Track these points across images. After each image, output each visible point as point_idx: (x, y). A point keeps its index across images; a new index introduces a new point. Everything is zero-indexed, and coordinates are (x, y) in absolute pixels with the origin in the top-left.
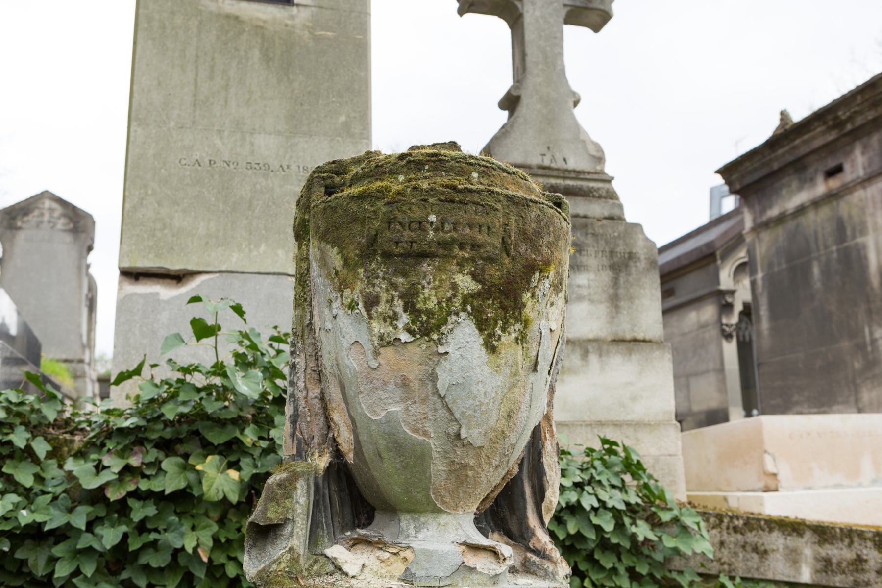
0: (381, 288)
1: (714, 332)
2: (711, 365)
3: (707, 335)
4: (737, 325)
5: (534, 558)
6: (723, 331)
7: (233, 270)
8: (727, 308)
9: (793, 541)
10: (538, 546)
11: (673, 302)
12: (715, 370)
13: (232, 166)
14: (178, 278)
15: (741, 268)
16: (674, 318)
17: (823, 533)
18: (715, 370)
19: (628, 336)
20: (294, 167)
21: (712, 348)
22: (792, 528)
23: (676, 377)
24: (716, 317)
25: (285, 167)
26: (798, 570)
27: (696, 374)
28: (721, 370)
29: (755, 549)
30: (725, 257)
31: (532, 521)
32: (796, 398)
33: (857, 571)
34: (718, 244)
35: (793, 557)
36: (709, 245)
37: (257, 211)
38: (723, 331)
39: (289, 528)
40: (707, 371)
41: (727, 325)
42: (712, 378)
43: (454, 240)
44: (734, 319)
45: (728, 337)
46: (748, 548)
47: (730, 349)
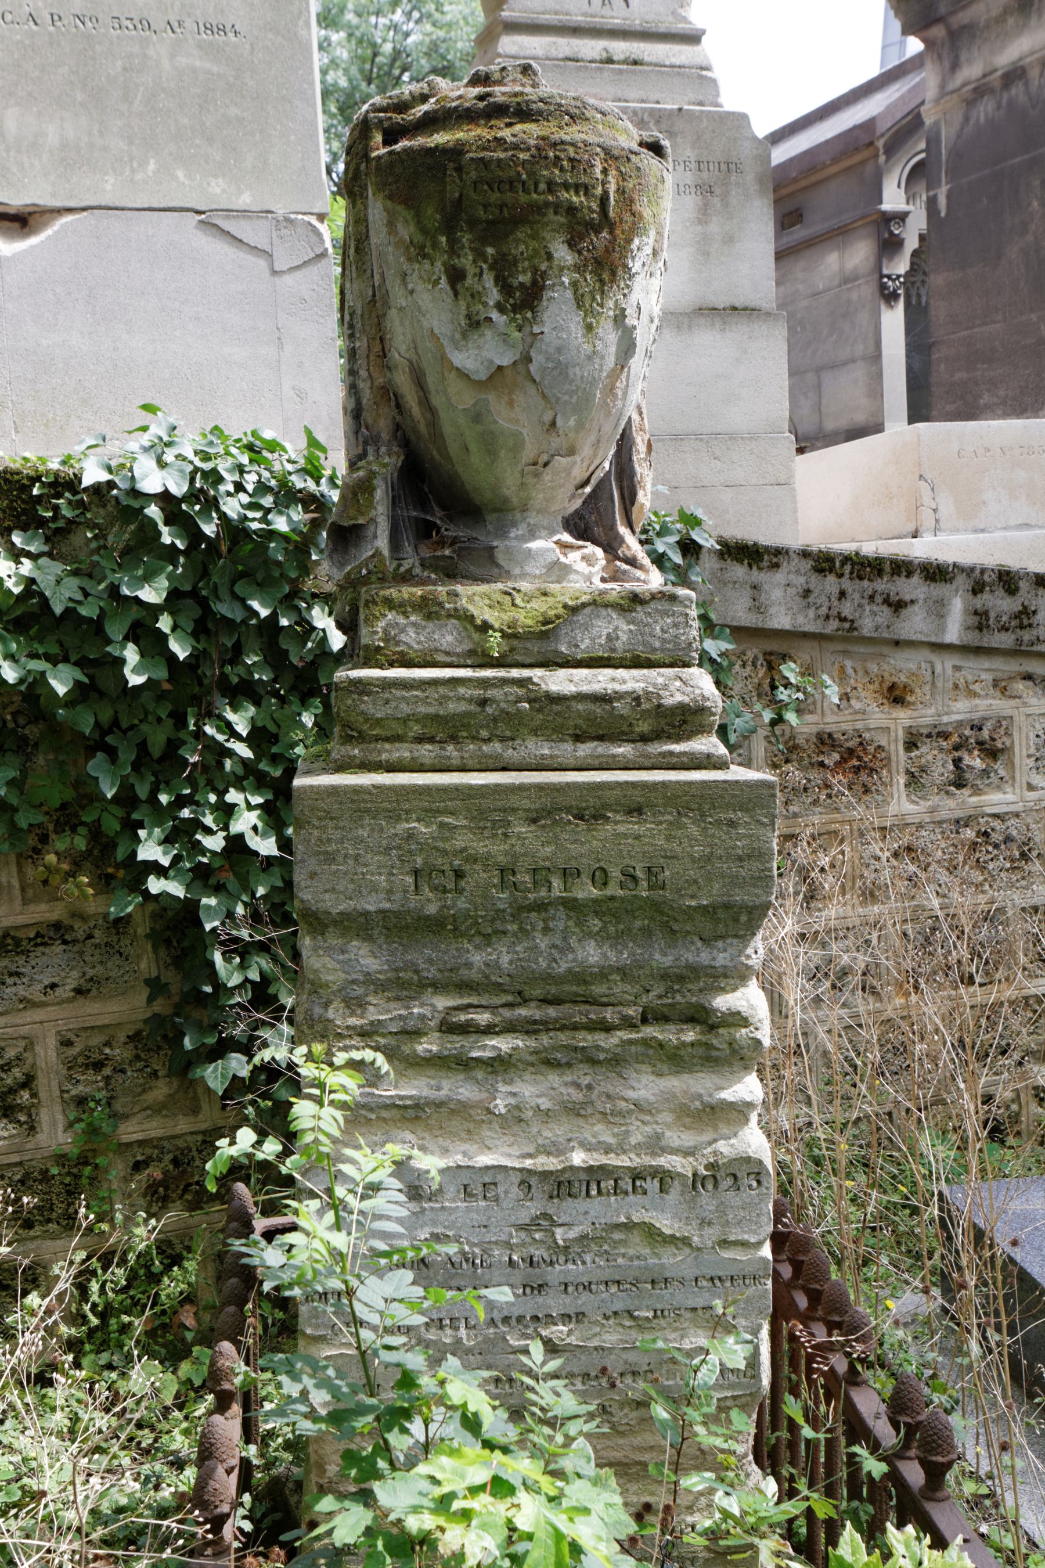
0: (466, 261)
1: (867, 290)
2: (859, 349)
3: (855, 295)
4: (907, 275)
5: (625, 567)
6: (883, 287)
7: (118, 204)
8: (891, 245)
9: (939, 590)
10: (628, 554)
11: (799, 233)
12: (864, 358)
13: (89, 24)
15: (917, 172)
16: (798, 267)
17: (980, 581)
18: (864, 358)
19: (722, 302)
20: (189, 24)
21: (863, 318)
22: (936, 573)
23: (793, 372)
24: (872, 260)
25: (175, 25)
26: (942, 629)
27: (834, 366)
28: (876, 357)
29: (887, 601)
30: (892, 148)
31: (623, 530)
32: (985, 399)
33: (1022, 627)
34: (882, 127)
35: (939, 610)
36: (868, 126)
37: (137, 103)
38: (883, 287)
39: (372, 528)
40: (853, 361)
41: (889, 277)
42: (859, 372)
43: (547, 204)
44: (901, 266)
45: (890, 298)
46: (879, 599)
47: (893, 322)
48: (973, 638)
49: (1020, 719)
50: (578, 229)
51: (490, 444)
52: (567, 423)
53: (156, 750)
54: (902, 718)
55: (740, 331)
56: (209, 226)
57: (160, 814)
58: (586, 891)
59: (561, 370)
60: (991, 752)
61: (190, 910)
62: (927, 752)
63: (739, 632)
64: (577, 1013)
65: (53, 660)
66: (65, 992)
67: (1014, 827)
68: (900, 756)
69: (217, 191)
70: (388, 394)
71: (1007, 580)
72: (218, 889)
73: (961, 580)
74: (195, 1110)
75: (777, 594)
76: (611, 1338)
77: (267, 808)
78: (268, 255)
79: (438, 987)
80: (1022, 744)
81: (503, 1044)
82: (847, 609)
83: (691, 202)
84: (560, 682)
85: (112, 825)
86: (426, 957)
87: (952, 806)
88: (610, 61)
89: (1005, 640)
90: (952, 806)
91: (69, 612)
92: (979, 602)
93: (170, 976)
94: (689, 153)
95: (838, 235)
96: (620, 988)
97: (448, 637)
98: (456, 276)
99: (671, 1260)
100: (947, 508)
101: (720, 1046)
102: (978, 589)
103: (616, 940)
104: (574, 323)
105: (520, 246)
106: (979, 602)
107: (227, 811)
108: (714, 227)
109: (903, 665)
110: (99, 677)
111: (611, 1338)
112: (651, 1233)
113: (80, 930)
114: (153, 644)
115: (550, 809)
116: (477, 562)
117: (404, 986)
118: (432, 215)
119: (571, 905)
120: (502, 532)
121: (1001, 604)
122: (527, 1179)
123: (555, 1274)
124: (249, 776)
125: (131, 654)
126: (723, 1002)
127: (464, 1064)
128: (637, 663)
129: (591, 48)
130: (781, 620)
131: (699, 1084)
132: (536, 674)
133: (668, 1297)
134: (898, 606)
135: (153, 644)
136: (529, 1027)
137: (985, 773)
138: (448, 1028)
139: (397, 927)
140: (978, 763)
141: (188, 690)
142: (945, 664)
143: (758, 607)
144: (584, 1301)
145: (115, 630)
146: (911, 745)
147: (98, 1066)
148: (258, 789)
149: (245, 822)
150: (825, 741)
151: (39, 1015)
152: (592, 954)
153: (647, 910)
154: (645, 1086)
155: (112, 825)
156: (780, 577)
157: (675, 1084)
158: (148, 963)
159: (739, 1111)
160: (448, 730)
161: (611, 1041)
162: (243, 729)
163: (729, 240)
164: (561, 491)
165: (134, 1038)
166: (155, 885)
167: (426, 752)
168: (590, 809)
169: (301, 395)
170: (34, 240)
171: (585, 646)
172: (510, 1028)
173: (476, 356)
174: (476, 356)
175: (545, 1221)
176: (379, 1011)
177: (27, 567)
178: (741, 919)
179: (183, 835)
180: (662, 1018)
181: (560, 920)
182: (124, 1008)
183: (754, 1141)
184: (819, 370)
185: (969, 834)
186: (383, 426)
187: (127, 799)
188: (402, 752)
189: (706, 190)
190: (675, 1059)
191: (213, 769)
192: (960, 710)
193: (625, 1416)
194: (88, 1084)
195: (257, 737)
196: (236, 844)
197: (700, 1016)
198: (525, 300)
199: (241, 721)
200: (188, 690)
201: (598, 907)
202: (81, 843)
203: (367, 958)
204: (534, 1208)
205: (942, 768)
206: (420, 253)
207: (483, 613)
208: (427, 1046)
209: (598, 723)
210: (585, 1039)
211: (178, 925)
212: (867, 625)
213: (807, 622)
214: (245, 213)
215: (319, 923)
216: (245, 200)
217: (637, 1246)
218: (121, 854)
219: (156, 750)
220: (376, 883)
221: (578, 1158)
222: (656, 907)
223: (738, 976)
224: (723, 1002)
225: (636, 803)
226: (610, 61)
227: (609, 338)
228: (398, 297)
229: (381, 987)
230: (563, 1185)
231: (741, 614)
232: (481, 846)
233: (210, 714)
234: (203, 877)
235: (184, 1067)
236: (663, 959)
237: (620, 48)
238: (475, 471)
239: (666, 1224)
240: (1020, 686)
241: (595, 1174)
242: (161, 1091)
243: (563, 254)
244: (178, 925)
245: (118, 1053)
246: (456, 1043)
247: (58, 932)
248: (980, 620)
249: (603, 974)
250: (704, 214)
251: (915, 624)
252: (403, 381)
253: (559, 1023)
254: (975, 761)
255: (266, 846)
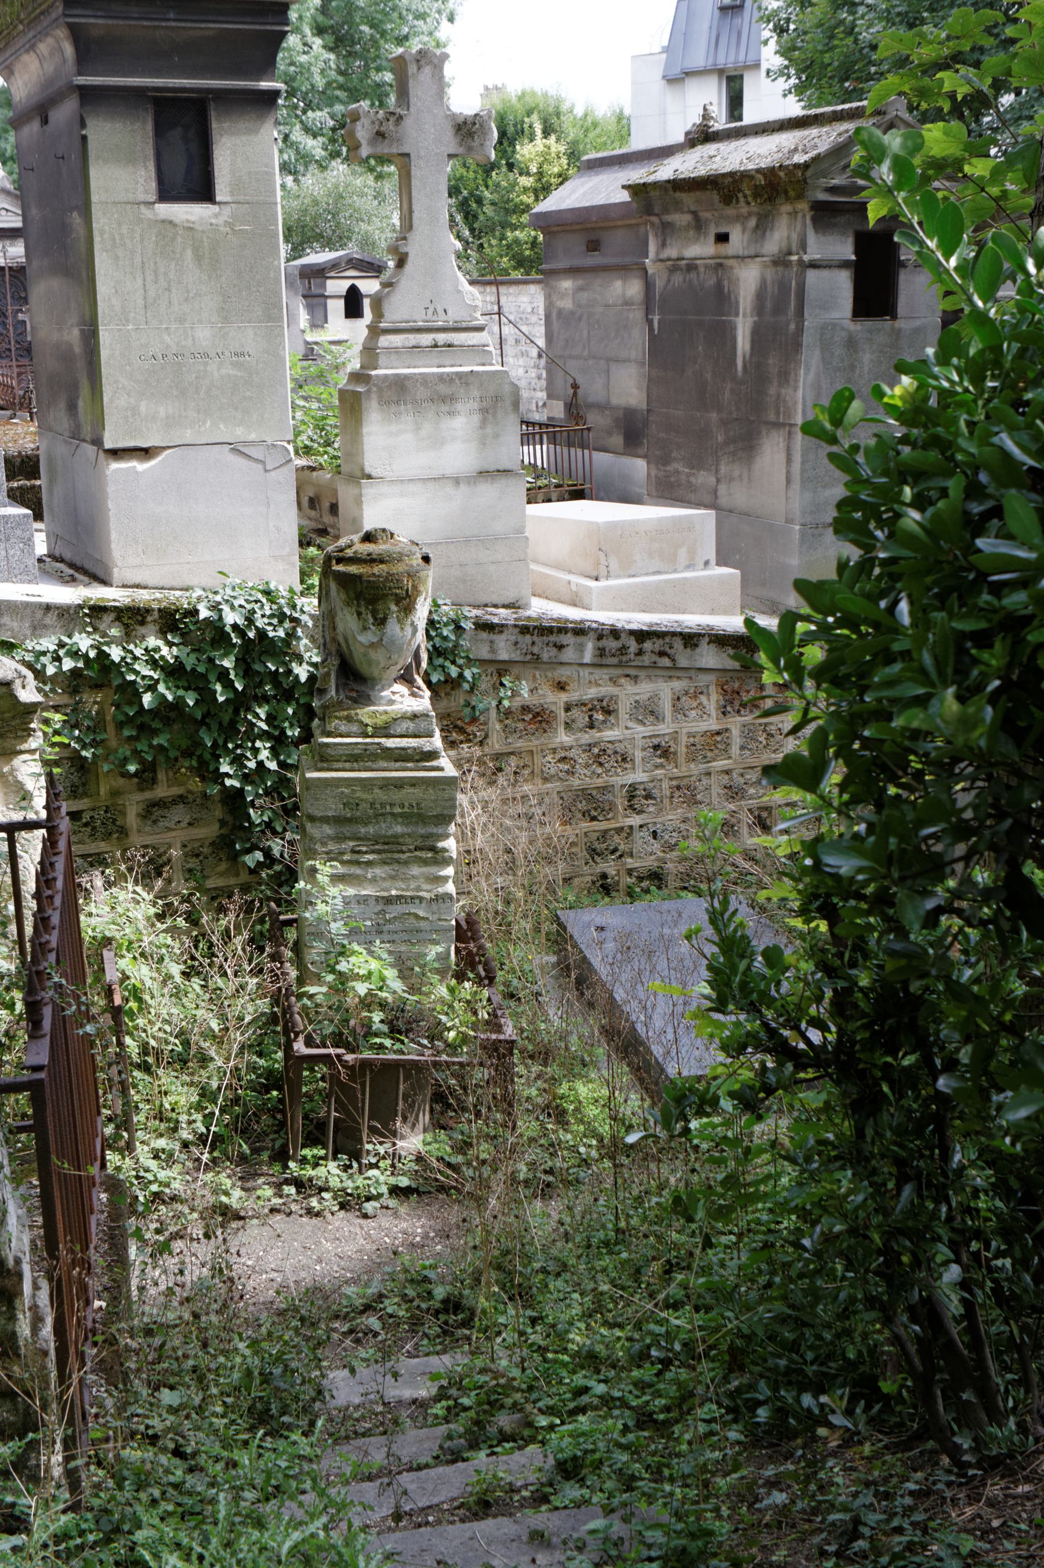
9: (580, 639)
14: (145, 453)
35: (581, 648)
48: (597, 660)
49: (622, 696)
50: (398, 600)
51: (370, 663)
52: (395, 657)
53: (225, 723)
54: (564, 697)
55: (502, 483)
56: (236, 451)
57: (228, 752)
58: (397, 810)
59: (393, 642)
60: (607, 712)
61: (240, 792)
62: (575, 713)
63: (482, 662)
64: (394, 847)
65: (186, 689)
66: (184, 824)
67: (620, 747)
68: (562, 715)
69: (239, 433)
70: (334, 640)
71: (615, 633)
72: (252, 783)
73: (591, 634)
74: (237, 875)
75: (502, 644)
76: (403, 948)
77: (272, 748)
78: (263, 463)
79: (350, 839)
80: (624, 708)
81: (370, 857)
82: (536, 650)
83: (476, 418)
84: (391, 743)
85: (207, 756)
86: (347, 830)
87: (586, 738)
88: (436, 346)
89: (614, 661)
90: (586, 738)
91: (194, 670)
92: (601, 644)
93: (229, 818)
94: (476, 393)
95: (622, 270)
96: (408, 840)
97: (354, 728)
98: (359, 614)
99: (423, 924)
100: (614, 564)
101: (440, 858)
102: (600, 637)
103: (407, 825)
104: (397, 628)
105: (380, 606)
106: (601, 644)
107: (256, 751)
108: (489, 430)
109: (563, 673)
110: (206, 696)
111: (403, 948)
112: (417, 916)
113: (191, 798)
114: (228, 685)
115: (386, 784)
116: (364, 699)
117: (340, 838)
118: (352, 594)
119: (392, 814)
120: (373, 688)
121: (612, 644)
122: (377, 899)
123: (386, 928)
124: (264, 735)
125: (218, 687)
126: (440, 845)
127: (358, 863)
128: (415, 736)
129: (426, 339)
130: (504, 656)
131: (432, 870)
132: (382, 740)
133: (421, 936)
134: (560, 647)
135: (228, 685)
136: (378, 852)
137: (604, 722)
138: (353, 852)
139: (338, 821)
140: (601, 717)
141: (240, 703)
142: (585, 673)
143: (493, 651)
144: (395, 937)
145: (212, 677)
146: (568, 709)
147: (197, 856)
148: (268, 740)
149: (264, 754)
150: (525, 709)
151: (174, 834)
152: (399, 829)
153: (416, 816)
154: (415, 870)
155: (207, 756)
156: (503, 637)
157: (425, 870)
158: (218, 812)
159: (445, 879)
160: (356, 758)
161: (404, 856)
162: (263, 716)
163: (496, 436)
164: (394, 671)
165: (212, 844)
166: (228, 782)
167: (347, 765)
168: (399, 784)
169: (278, 529)
170: (153, 463)
171: (399, 730)
172: (373, 852)
173: (365, 638)
174: (365, 638)
175: (383, 912)
176: (332, 846)
177: (175, 649)
178: (445, 818)
179: (238, 761)
180: (421, 849)
181: (389, 819)
182: (209, 831)
183: (450, 888)
184: (609, 360)
185: (596, 750)
186: (333, 649)
187: (215, 744)
188: (340, 765)
189: (484, 411)
190: (425, 862)
191: (252, 734)
192: (592, 693)
193: (407, 973)
194: (193, 863)
195: (270, 719)
196: (260, 764)
197: (433, 849)
198: (381, 622)
199: (262, 712)
200: (240, 703)
201: (401, 815)
202: (195, 763)
203: (328, 830)
204: (379, 908)
205: (582, 719)
206: (348, 604)
207: (367, 720)
208: (346, 857)
209: (402, 756)
210: (396, 856)
211: (234, 800)
212: (545, 657)
213: (516, 656)
214: (252, 443)
215: (312, 819)
216: (253, 437)
217: (412, 920)
218: (212, 768)
219: (225, 723)
220: (332, 807)
221: (394, 892)
222: (419, 815)
223: (447, 836)
224: (440, 845)
225: (414, 782)
226: (436, 346)
227: (409, 630)
228: (340, 615)
229: (332, 839)
230: (389, 901)
231: (484, 653)
232: (364, 796)
233: (249, 709)
234: (246, 778)
235: (234, 857)
236: (422, 830)
237: (442, 338)
238: (364, 669)
239: (421, 913)
240: (623, 680)
241: (399, 898)
242: (223, 866)
243: (394, 608)
244: (234, 800)
245: (206, 850)
246: (356, 857)
247: (181, 799)
248: (601, 652)
249: (403, 835)
250: (484, 423)
251: (568, 655)
252: (341, 639)
253: (390, 849)
254: (599, 716)
255: (272, 766)
